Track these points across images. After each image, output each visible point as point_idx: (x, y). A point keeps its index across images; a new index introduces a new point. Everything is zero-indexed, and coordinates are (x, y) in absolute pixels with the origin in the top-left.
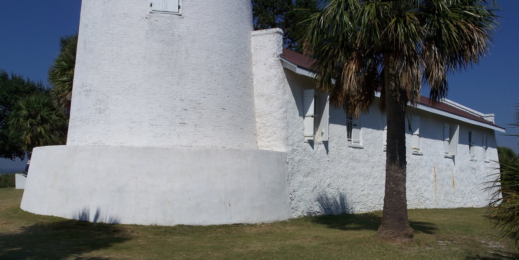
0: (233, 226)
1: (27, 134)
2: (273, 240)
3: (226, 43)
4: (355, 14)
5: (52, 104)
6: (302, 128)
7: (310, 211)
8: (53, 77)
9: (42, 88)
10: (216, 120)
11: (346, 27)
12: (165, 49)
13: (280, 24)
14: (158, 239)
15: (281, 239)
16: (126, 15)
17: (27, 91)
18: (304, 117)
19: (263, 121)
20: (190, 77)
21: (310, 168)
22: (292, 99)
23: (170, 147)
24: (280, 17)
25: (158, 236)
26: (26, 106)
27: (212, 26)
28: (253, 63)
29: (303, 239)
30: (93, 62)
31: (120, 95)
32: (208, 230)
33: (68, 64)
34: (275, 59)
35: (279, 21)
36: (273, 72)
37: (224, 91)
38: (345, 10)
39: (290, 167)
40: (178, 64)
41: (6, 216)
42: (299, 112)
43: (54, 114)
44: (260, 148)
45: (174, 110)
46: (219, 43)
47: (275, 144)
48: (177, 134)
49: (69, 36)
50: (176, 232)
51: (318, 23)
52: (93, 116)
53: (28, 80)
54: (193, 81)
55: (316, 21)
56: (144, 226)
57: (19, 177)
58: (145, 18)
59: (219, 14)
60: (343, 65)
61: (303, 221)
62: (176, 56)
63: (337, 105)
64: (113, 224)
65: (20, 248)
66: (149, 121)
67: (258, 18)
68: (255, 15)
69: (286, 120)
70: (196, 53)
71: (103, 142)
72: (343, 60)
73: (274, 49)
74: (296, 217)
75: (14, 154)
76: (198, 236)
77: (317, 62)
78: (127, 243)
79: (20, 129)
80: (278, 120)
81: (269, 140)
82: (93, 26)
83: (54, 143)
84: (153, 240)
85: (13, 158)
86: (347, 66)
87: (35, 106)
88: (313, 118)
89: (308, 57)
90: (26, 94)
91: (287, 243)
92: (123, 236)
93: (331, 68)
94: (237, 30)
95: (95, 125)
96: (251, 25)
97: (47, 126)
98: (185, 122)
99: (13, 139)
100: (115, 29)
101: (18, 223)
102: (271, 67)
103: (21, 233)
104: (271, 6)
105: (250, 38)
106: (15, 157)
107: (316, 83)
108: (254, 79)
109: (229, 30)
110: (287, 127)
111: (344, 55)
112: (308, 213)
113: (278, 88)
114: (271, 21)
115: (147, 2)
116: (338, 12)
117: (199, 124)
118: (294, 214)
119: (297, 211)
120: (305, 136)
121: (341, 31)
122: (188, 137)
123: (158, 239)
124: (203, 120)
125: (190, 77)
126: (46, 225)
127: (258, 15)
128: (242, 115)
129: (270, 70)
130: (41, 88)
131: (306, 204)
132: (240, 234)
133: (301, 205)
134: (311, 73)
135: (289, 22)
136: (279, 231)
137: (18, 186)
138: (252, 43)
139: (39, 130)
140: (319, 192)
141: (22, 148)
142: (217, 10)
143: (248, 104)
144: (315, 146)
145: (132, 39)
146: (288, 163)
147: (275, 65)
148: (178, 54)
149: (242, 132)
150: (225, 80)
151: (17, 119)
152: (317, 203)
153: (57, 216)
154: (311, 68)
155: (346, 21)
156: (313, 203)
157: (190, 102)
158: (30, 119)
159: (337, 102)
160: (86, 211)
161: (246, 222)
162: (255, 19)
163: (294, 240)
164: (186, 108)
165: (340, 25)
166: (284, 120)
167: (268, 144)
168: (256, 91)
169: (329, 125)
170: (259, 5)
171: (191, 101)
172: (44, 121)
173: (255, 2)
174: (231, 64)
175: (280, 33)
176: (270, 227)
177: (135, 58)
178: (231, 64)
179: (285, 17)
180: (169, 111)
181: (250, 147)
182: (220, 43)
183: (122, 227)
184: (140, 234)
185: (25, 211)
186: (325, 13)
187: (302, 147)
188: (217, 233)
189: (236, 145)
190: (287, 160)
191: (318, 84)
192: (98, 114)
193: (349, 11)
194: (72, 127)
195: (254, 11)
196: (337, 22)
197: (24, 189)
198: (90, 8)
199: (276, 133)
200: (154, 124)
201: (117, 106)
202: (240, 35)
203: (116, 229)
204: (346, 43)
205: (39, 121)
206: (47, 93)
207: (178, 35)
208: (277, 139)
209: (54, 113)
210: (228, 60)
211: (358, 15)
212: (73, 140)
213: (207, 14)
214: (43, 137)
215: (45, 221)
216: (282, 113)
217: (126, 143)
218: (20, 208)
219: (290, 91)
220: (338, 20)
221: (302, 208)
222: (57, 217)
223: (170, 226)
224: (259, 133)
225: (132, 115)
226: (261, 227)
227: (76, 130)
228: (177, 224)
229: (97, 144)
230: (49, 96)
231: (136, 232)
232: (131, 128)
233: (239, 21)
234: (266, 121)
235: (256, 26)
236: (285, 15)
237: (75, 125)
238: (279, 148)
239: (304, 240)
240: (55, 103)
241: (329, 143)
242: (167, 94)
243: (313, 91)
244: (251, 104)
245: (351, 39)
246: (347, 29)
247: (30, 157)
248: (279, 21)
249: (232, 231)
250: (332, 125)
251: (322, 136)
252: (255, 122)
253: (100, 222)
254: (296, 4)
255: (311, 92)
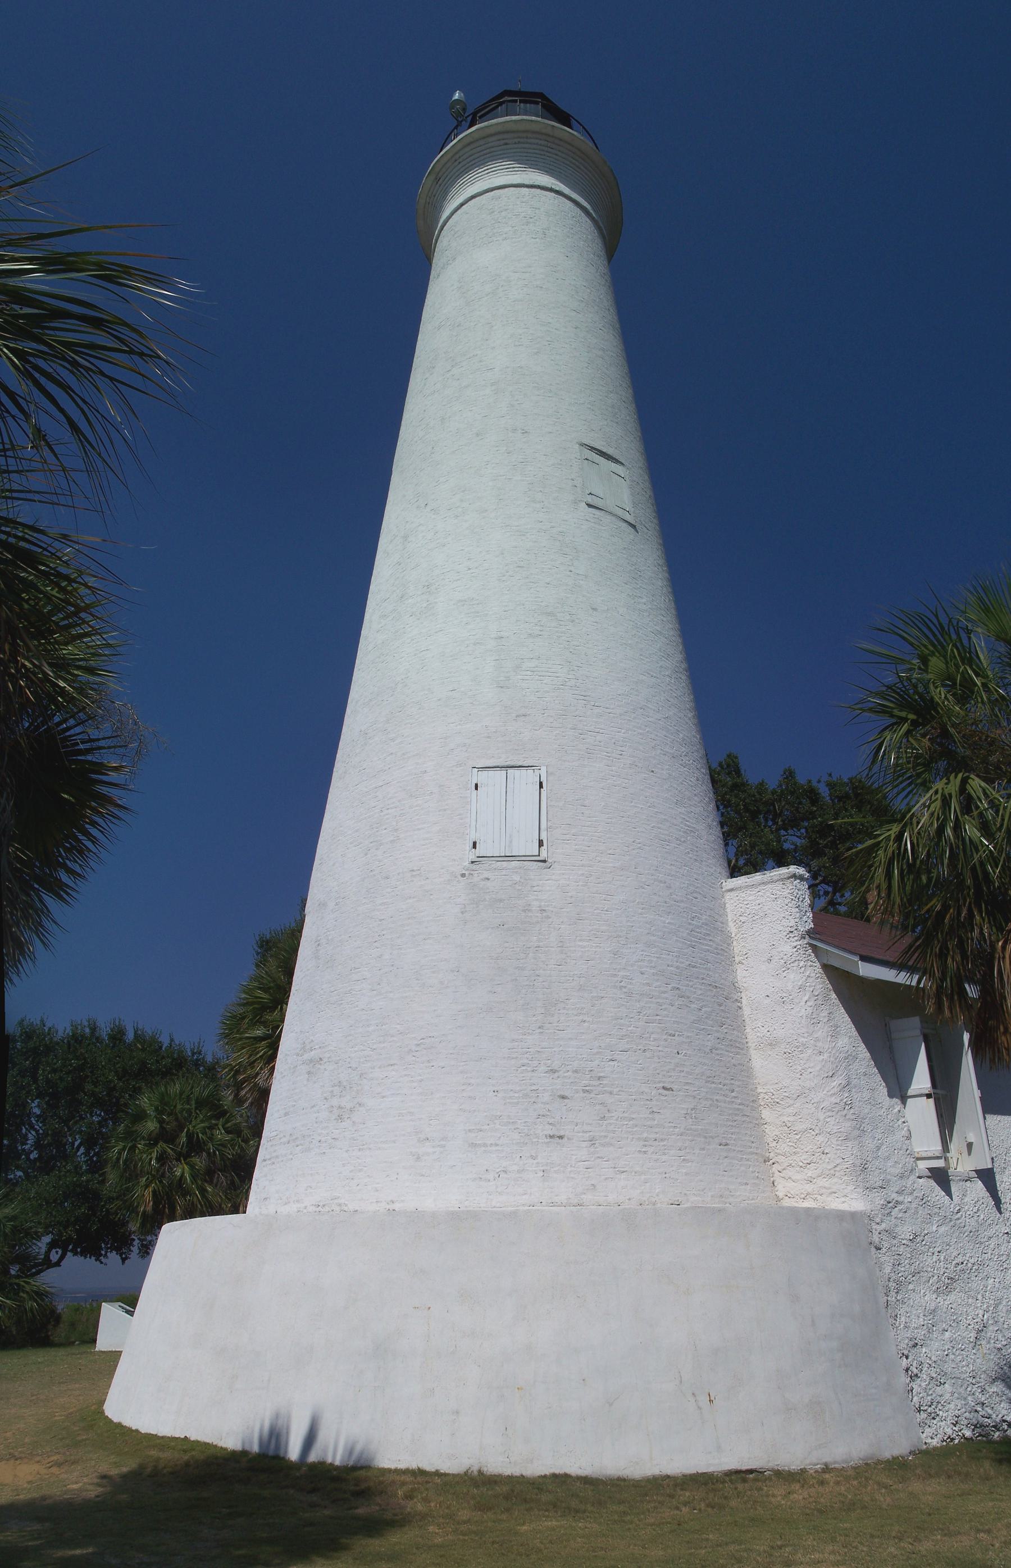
0: (727, 1479)
1: (147, 1186)
2: (872, 1536)
3: (661, 916)
4: (994, 818)
5: (219, 1100)
6: (904, 1132)
7: (981, 1419)
8: (230, 1029)
9: (199, 1060)
10: (649, 1123)
11: (977, 851)
12: (506, 945)
13: (795, 850)
14: (490, 1524)
15: (899, 1531)
16: (414, 873)
17: (164, 1070)
18: (904, 1099)
19: (785, 1119)
20: (573, 1009)
21: (954, 1262)
22: (860, 1049)
23: (521, 1208)
24: (794, 835)
25: (489, 1514)
26: (157, 1109)
27: (622, 878)
28: (737, 959)
29: (978, 1531)
30: (332, 989)
31: (393, 1067)
32: (646, 1495)
33: (271, 995)
34: (795, 944)
35: (793, 844)
36: (794, 978)
37: (666, 1040)
38: (963, 814)
39: (887, 1261)
40: (541, 979)
41: (63, 1438)
42: (886, 1085)
43: (220, 1127)
44: (787, 1203)
45: (533, 1100)
46: (644, 917)
47: (830, 1188)
48: (540, 1170)
49: (279, 929)
50: (544, 1498)
51: (899, 848)
52: (322, 1129)
53: (172, 1040)
54: (581, 1018)
55: (891, 843)
56: (445, 1475)
57: (110, 1313)
58: (460, 877)
59: (640, 848)
60: (993, 946)
61: (964, 1457)
62: (536, 959)
63: (999, 1059)
64: (355, 1468)
65: (90, 1550)
66: (466, 1133)
67: (737, 843)
68: (728, 836)
69: (852, 1111)
70: (584, 947)
71: (342, 1201)
72: (990, 935)
73: (790, 918)
74: (935, 1442)
75: (108, 1244)
76: (616, 1517)
77: (914, 944)
78: (395, 1539)
79: (131, 1173)
80: (828, 1114)
81: (809, 1174)
82: (337, 904)
83: (212, 1209)
84: (474, 1528)
85: (101, 1255)
86: (1004, 948)
87: (179, 1107)
88: (931, 1101)
89: (887, 929)
90: (162, 1078)
91: (925, 1546)
92: (383, 1510)
93: (958, 958)
94: (687, 882)
95: (324, 1153)
96: (720, 865)
97: (200, 1162)
98: (562, 1133)
99: (111, 1200)
100: (387, 908)
101: (93, 1463)
102: (786, 967)
103: (97, 1496)
104: (768, 812)
105: (723, 897)
106: (108, 1254)
107: (923, 1002)
108: (744, 1001)
109: (665, 883)
110: (857, 1133)
111: (989, 922)
112: (976, 1426)
113: (814, 1021)
114: (771, 847)
115: (466, 840)
116: (945, 820)
117: (601, 1137)
118: (927, 1430)
119: (938, 1419)
120: (917, 1155)
121: (966, 862)
122: (572, 1176)
123: (490, 1524)
124: (611, 1124)
125: (573, 1009)
126: (165, 1471)
127: (735, 837)
128: (719, 1104)
129: (785, 974)
130: (198, 1060)
131: (962, 1390)
132: (756, 1509)
133: (947, 1396)
134: (903, 974)
135: (819, 844)
136: (889, 1500)
137: (104, 1342)
138: (729, 907)
139: (178, 1174)
140: (999, 1346)
141: (130, 1225)
142: (632, 840)
143: (733, 1071)
144: (954, 1188)
145: (426, 927)
146: (878, 1249)
147: (797, 958)
148: (540, 955)
149: (725, 1154)
150: (665, 1009)
151: (129, 1145)
152: (998, 1387)
153: (199, 1439)
154: (899, 961)
155: (975, 840)
156: (987, 1388)
157: (576, 1075)
158: (161, 1143)
159: (996, 1050)
160: (280, 1422)
161: (771, 1465)
162: (730, 844)
163: (945, 1535)
164: (562, 1093)
165: (958, 847)
166: (845, 1112)
167: (809, 1188)
168: (753, 1035)
169: (985, 1118)
170: (737, 812)
171: (576, 1071)
172: (195, 1146)
173: (725, 807)
174: (677, 968)
175: (801, 878)
176: (855, 1483)
177: (434, 972)
178: (677, 968)
179: (807, 832)
180: (518, 1103)
181: (753, 1199)
182: (645, 916)
183: (381, 1479)
184: (432, 1504)
185: (115, 1423)
186: (911, 824)
187: (915, 1194)
188: (677, 1508)
189: (710, 1194)
190: (876, 1238)
191: (928, 1003)
192: (336, 1121)
193: (975, 813)
194: (265, 1160)
195: (725, 827)
196: (948, 843)
197: (121, 1352)
198: (334, 865)
199: (826, 1151)
200: (477, 1142)
201: (383, 1097)
202: (696, 892)
203: (363, 1486)
204: (989, 888)
205: (182, 1149)
206: (211, 1071)
207: (540, 907)
208: (832, 1172)
209: (220, 1123)
210: (668, 957)
211: (1003, 820)
212: (265, 1199)
213: (609, 852)
214: (185, 1193)
215: (166, 1455)
216: (835, 1090)
217: (403, 1201)
218: (103, 1412)
219: (849, 1026)
220: (952, 837)
221: (952, 1406)
222: (198, 1442)
223: (524, 1474)
224: (778, 1154)
225: (420, 1119)
226: (822, 1483)
227: (275, 1169)
228: (547, 1471)
229: (327, 1209)
230: (214, 1079)
231: (422, 1498)
232: (418, 1158)
233: (691, 858)
234: (791, 1119)
235: (734, 861)
236: (806, 828)
237: (274, 1154)
238: (843, 1199)
239: (982, 1535)
240: (227, 1096)
241: (997, 1177)
242: (514, 1056)
243: (916, 1021)
244: (743, 1071)
245: (1000, 877)
246: (981, 857)
247: (147, 1250)
248: (793, 844)
249: (726, 1498)
250: (993, 1119)
251: (969, 1153)
252: (759, 1123)
253: (316, 1461)
254: (831, 799)
255: (911, 1027)
